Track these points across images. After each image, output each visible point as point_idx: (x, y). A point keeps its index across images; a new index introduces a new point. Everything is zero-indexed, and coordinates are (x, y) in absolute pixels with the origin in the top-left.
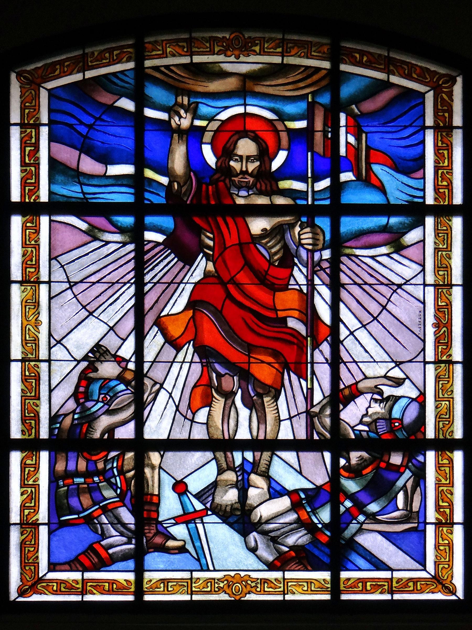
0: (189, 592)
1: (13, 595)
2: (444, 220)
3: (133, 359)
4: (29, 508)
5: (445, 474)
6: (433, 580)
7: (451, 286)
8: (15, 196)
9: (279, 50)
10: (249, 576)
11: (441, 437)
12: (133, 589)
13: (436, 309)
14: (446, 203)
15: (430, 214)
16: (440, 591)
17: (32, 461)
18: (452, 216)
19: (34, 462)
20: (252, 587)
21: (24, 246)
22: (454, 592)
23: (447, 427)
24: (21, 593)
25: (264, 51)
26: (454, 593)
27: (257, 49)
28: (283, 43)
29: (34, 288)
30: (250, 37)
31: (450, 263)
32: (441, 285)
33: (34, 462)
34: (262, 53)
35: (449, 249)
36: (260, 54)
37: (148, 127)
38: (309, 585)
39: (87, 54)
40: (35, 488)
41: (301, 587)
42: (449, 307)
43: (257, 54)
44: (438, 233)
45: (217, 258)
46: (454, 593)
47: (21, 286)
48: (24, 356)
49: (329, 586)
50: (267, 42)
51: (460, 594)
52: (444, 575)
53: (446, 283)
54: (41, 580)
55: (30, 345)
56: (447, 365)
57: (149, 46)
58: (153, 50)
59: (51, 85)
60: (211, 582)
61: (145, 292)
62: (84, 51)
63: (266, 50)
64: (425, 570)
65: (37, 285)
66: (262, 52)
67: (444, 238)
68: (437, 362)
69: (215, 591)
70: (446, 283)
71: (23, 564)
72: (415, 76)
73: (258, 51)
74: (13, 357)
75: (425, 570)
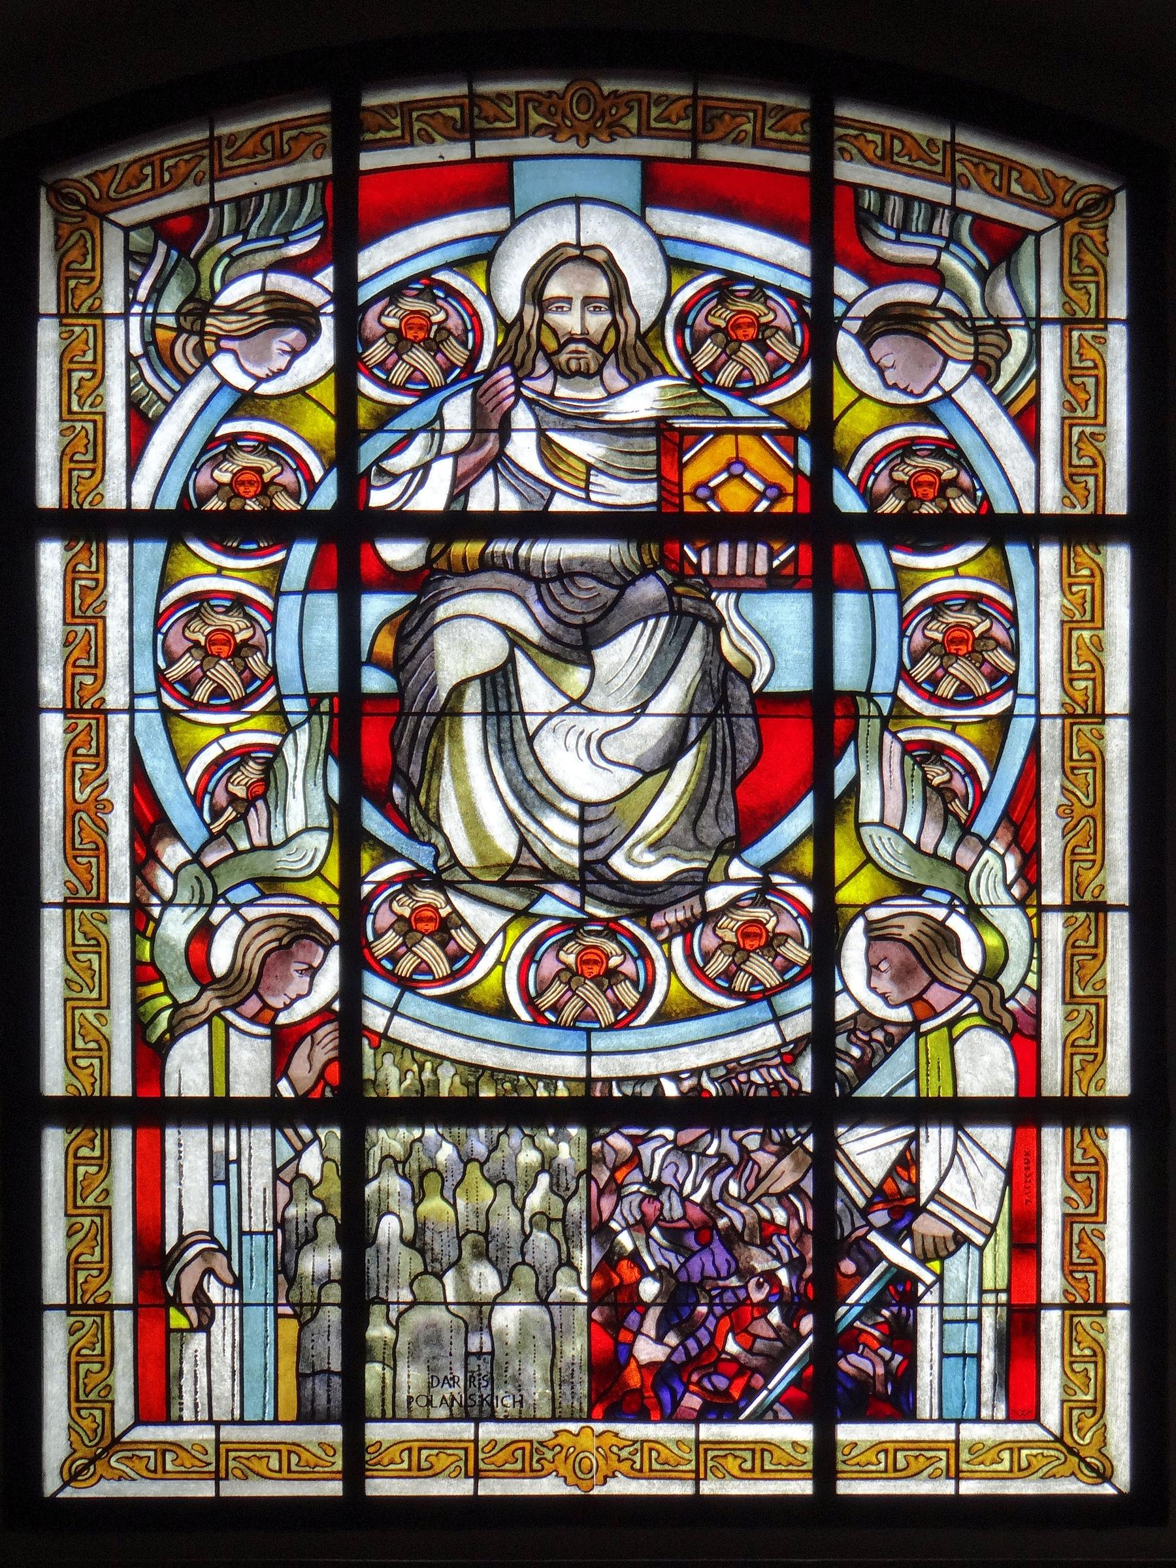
0: (471, 1472)
1: (51, 1484)
2: (1085, 552)
3: (330, 309)
4: (88, 1360)
5: (1084, 1380)
6: (1058, 1445)
7: (1103, 1308)
8: (48, 495)
9: (685, 125)
10: (616, 1435)
11: (1077, 1093)
12: (339, 1466)
13: (1066, 377)
14: (1090, 509)
15: (1052, 1121)
16: (1073, 1474)
17: (93, 1149)
18: (1108, 1125)
19: (97, 1153)
20: (620, 1461)
21: (71, 1211)
22: (1108, 1473)
23: (1090, 1069)
24: (71, 1477)
25: (649, 128)
26: (1104, 1476)
27: (632, 122)
28: (694, 106)
29: (98, 1320)
30: (615, 93)
31: (1103, 1149)
32: (1079, 716)
33: (97, 1153)
34: (644, 132)
35: (1100, 1214)
36: (639, 135)
37: (368, 708)
38: (758, 1456)
39: (219, 138)
40: (96, 625)
41: (739, 1461)
42: (1099, 1268)
43: (633, 135)
44: (1073, 1173)
45: (536, 416)
46: (1104, 1476)
47: (69, 1315)
48: (68, 894)
49: (809, 1457)
50: (657, 105)
51: (1123, 1476)
52: (1086, 1440)
53: (1090, 711)
54: (116, 1441)
55: (84, 860)
56: (1092, 915)
57: (369, 119)
58: (381, 128)
59: (126, 217)
60: (523, 1449)
61: (360, 302)
62: (212, 133)
63: (653, 124)
64: (1038, 235)
65: (107, 1313)
66: (645, 131)
67: (1084, 597)
68: (1068, 322)
69: (532, 1470)
70: (1090, 711)
71: (76, 1398)
72: (1016, 189)
73: (634, 131)
74: (42, 309)
75: (1038, 235)
